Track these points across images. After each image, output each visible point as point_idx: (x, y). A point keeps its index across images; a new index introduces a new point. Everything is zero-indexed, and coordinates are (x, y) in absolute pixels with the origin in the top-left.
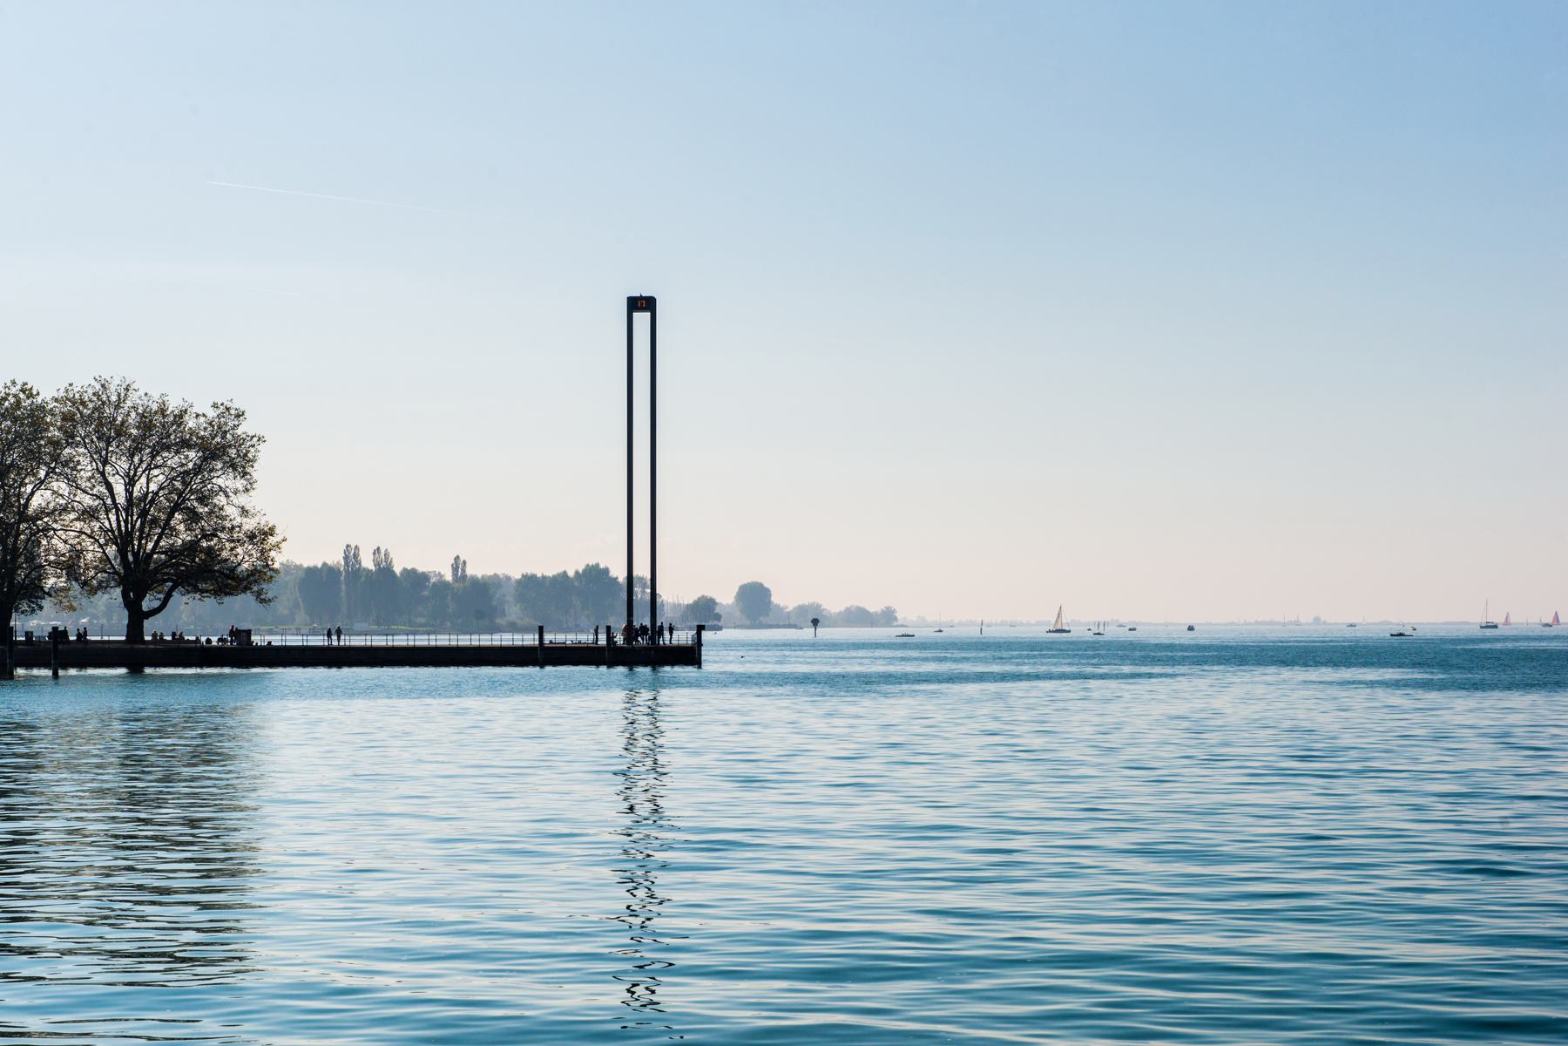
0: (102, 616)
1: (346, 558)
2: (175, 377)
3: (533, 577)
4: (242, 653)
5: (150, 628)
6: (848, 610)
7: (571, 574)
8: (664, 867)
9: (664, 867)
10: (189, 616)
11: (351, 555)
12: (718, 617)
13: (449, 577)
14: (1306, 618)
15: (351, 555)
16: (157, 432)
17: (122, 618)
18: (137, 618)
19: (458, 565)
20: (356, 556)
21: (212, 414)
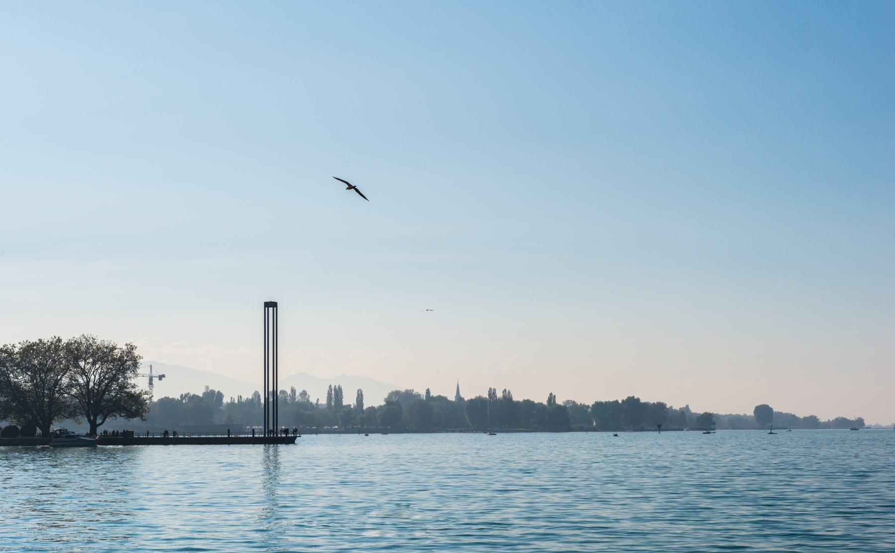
0: (81, 427)
1: (489, 395)
2: (111, 334)
3: (601, 403)
4: (128, 439)
5: (100, 430)
6: (837, 419)
7: (620, 402)
8: (264, 502)
9: (264, 502)
10: (113, 424)
11: (492, 393)
12: (714, 424)
13: (545, 403)
14: (742, 414)
15: (492, 393)
16: (103, 355)
17: (88, 426)
18: (94, 426)
19: (552, 398)
20: (494, 393)
21: (125, 348)
